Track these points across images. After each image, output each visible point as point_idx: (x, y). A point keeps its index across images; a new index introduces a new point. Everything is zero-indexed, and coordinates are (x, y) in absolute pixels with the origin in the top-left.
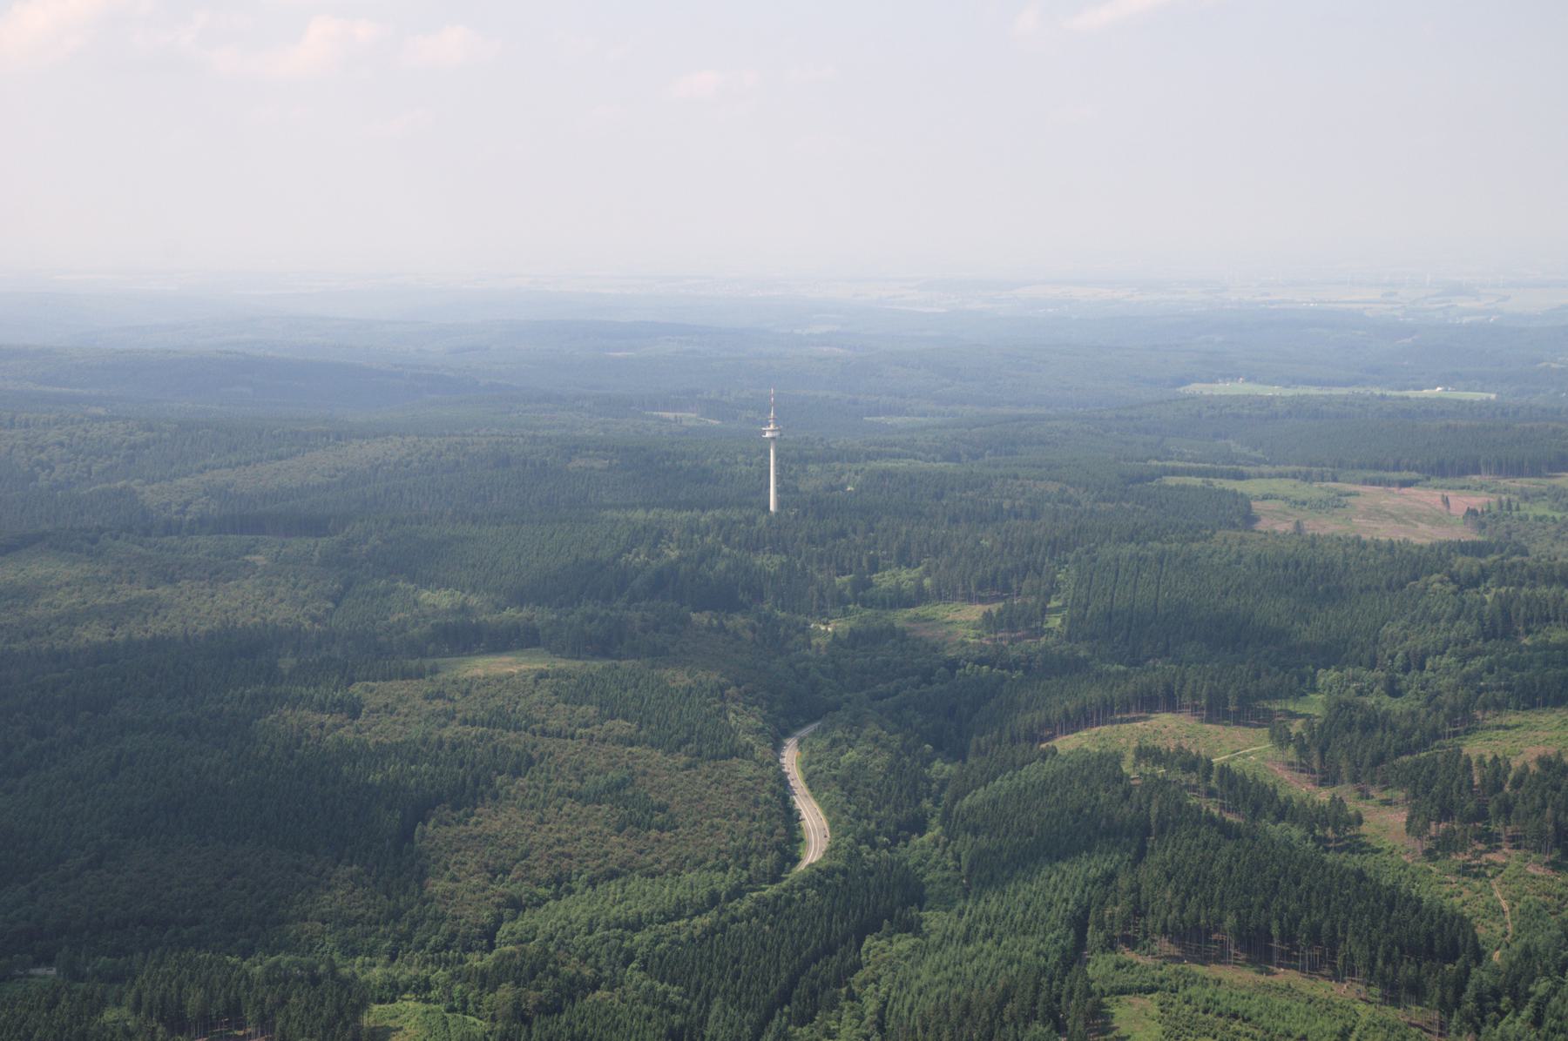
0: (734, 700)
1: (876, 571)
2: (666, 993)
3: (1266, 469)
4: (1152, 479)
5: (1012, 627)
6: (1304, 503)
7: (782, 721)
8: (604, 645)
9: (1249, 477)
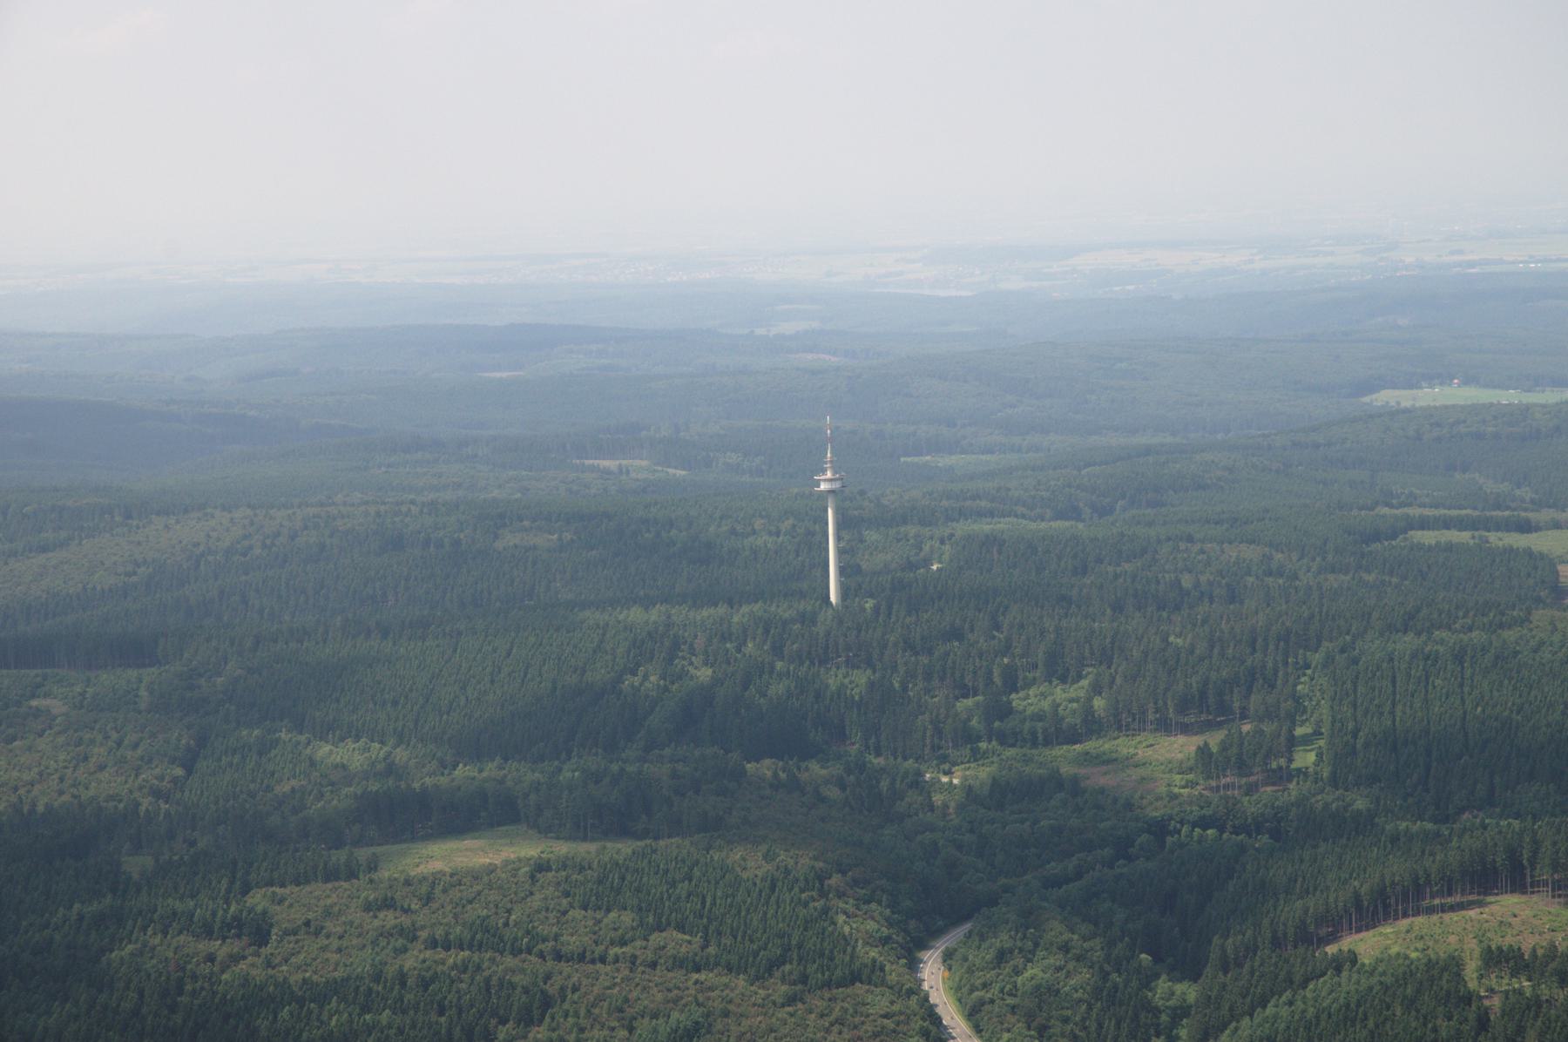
0: (841, 895)
1: (1015, 689)
4: (1394, 537)
5: (1242, 767)
7: (912, 924)
9: (1538, 529)
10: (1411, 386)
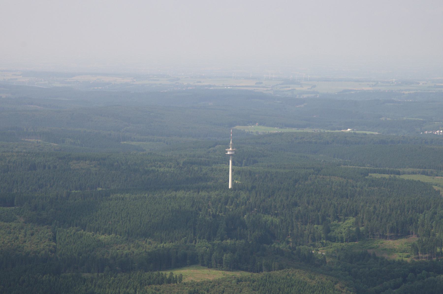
10: (245, 125)
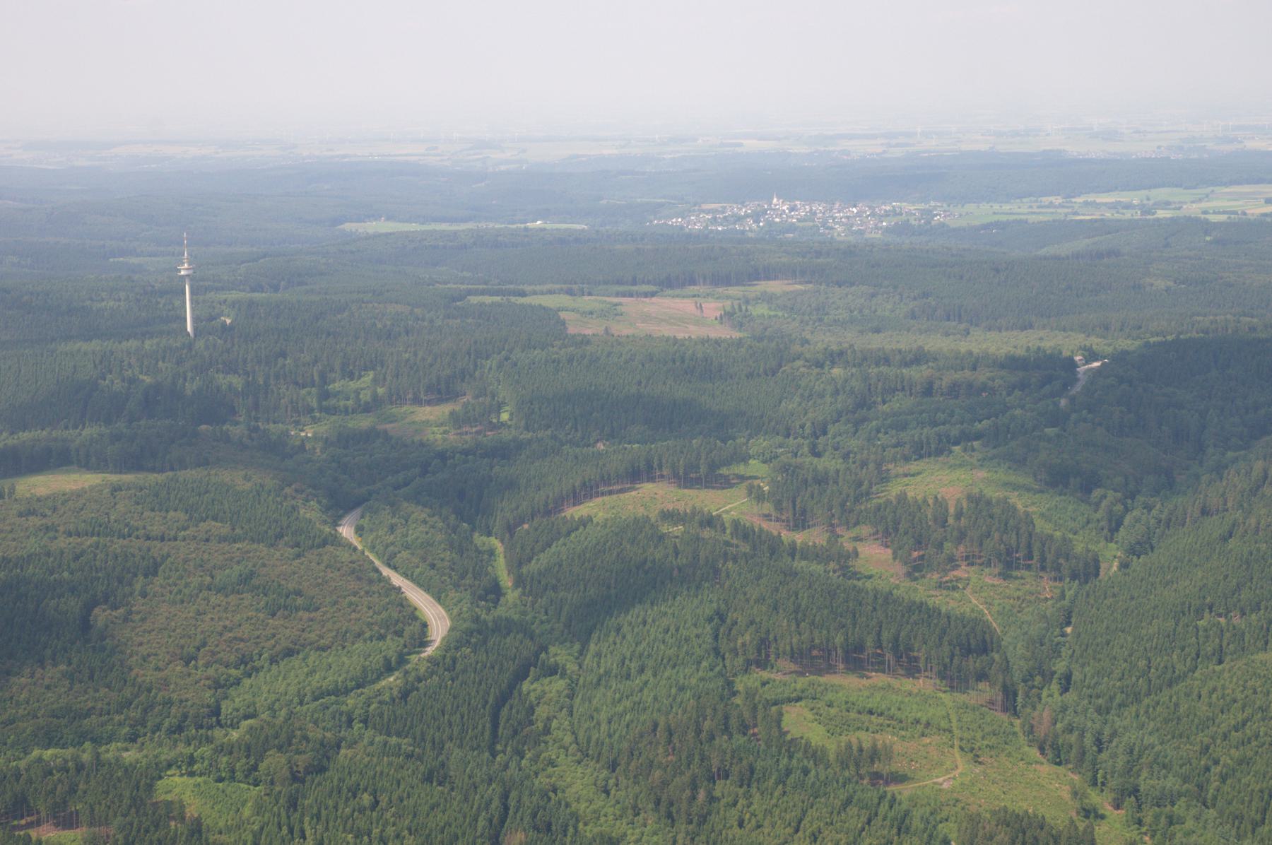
2: (399, 746)
3: (538, 288)
6: (591, 313)
8: (132, 463)
10: (359, 221)
